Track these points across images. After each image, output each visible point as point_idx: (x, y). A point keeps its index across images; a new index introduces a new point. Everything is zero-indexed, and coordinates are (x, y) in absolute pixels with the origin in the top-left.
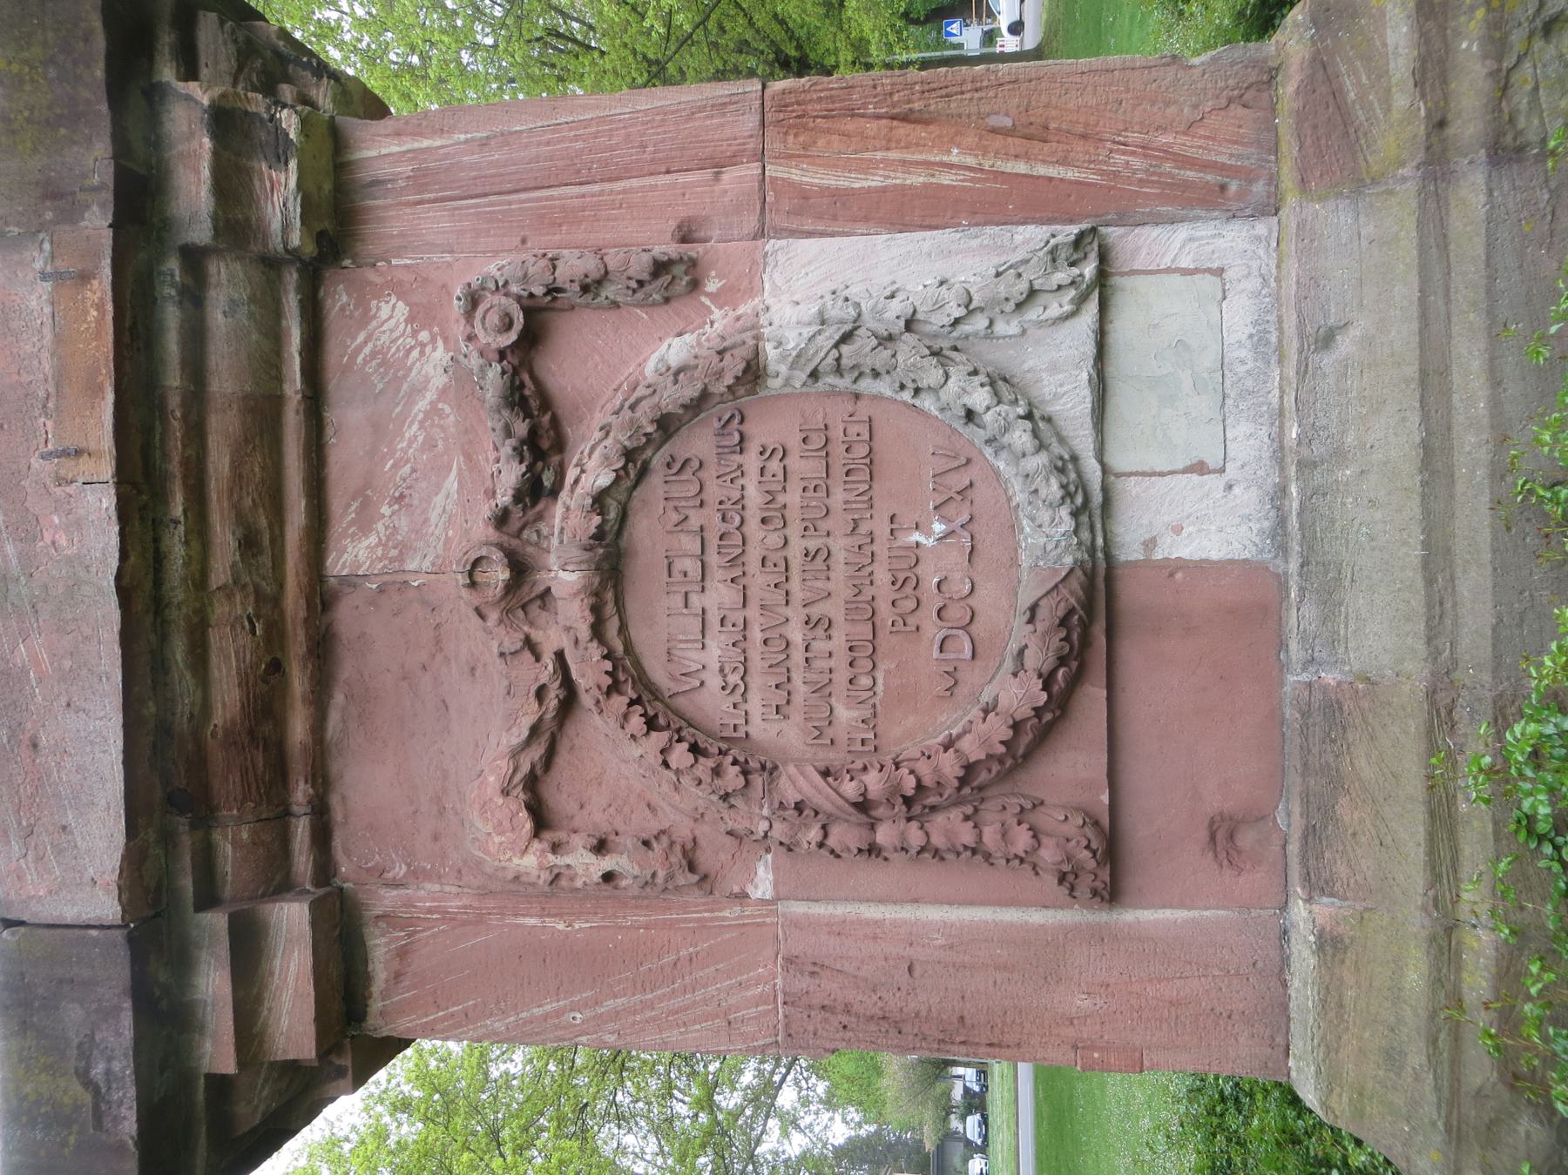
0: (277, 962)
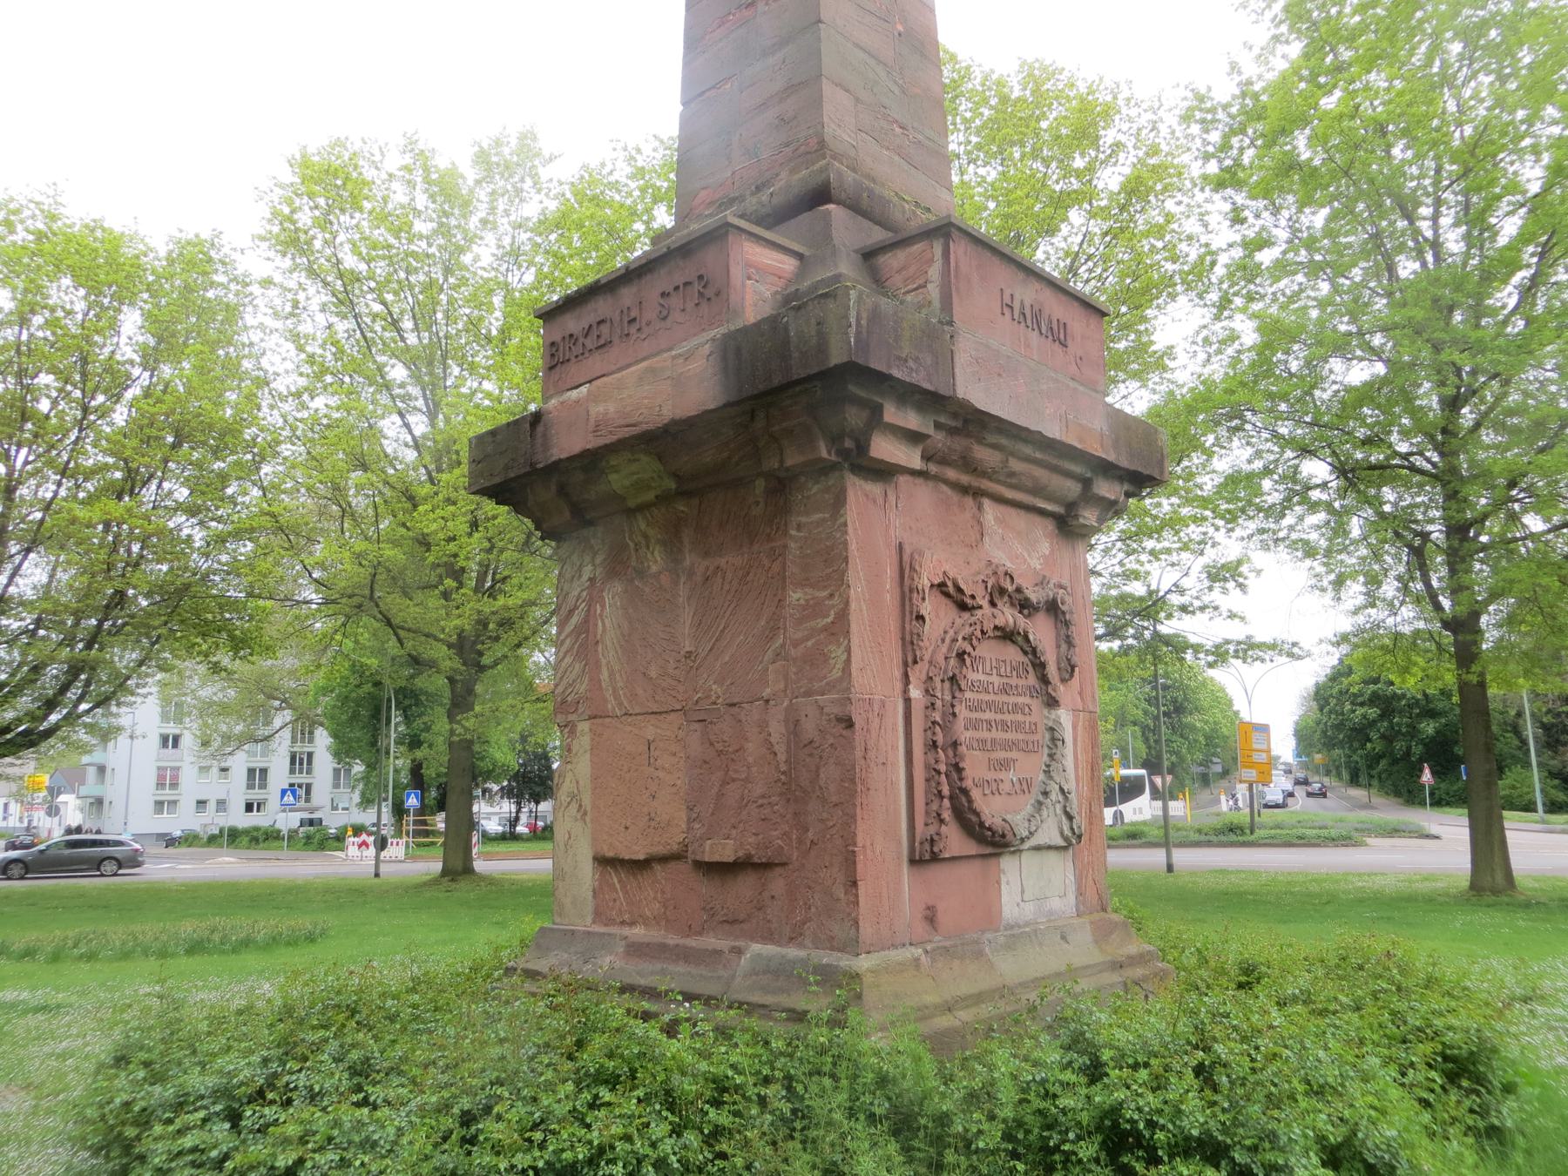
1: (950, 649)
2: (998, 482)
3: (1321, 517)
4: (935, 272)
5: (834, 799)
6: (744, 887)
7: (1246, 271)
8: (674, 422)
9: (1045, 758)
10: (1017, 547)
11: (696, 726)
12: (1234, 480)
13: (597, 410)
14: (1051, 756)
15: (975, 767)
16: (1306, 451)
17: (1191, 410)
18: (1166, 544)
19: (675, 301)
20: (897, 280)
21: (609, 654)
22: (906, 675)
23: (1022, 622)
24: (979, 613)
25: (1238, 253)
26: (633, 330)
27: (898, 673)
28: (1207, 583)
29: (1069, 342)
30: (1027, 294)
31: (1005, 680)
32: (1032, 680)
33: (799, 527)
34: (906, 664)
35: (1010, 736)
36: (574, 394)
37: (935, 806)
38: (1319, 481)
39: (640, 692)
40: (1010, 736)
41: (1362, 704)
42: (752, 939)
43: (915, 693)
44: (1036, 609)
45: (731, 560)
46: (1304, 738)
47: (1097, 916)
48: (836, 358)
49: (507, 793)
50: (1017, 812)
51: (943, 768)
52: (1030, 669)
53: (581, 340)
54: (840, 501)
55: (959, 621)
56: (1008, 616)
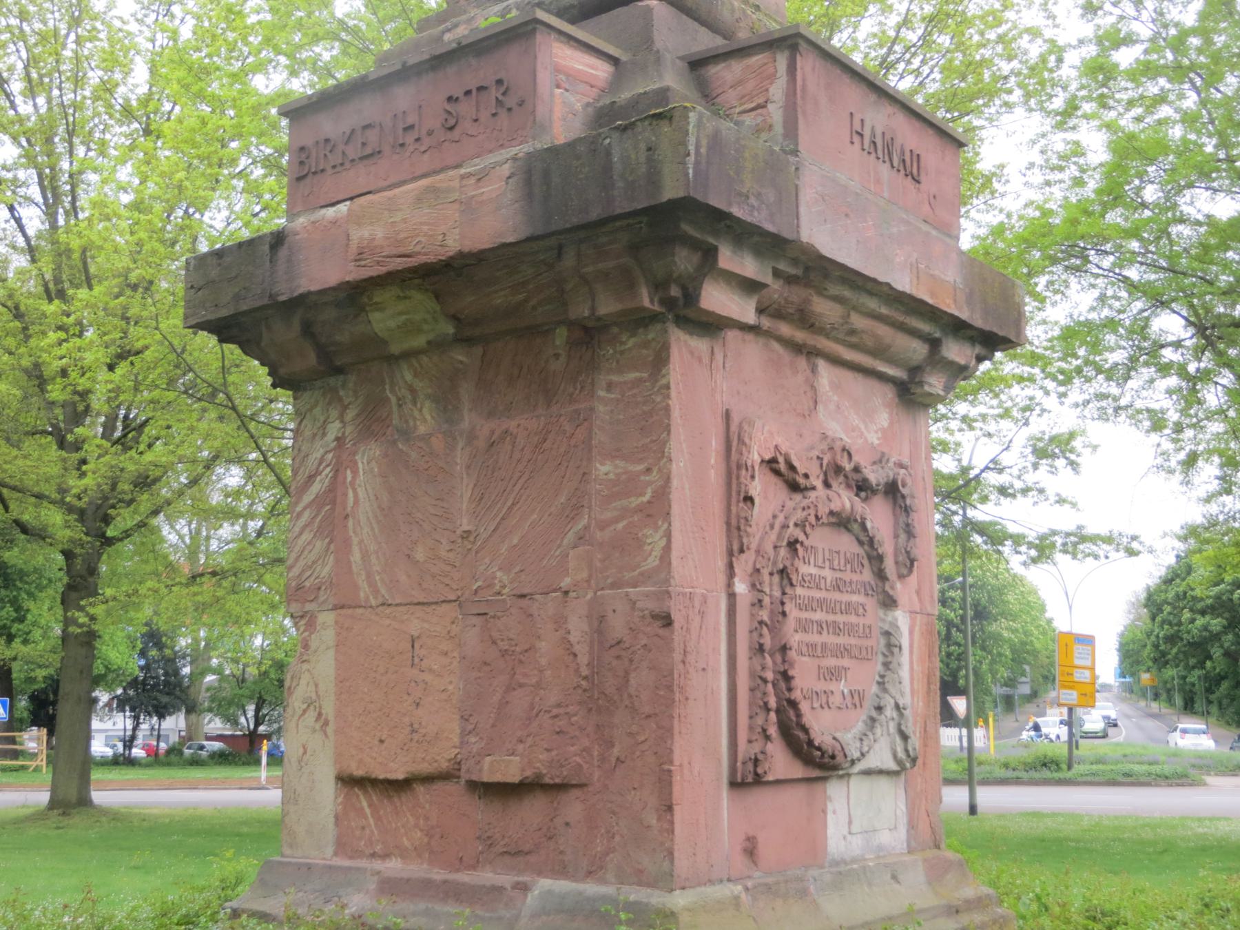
0: (736, 298)
1: (780, 537)
2: (837, 340)
3: (1173, 381)
4: (777, 90)
5: (647, 709)
6: (532, 811)
7: (1100, 72)
8: (461, 255)
9: (880, 668)
10: (853, 417)
11: (475, 620)
12: (1073, 334)
13: (360, 234)
14: (886, 665)
15: (805, 677)
16: (1160, 303)
17: (1028, 243)
18: (982, 409)
19: (465, 109)
20: (730, 97)
21: (363, 528)
22: (730, 566)
23: (860, 507)
24: (812, 494)
25: (1091, 50)
26: (409, 139)
27: (721, 564)
28: (1031, 458)
29: (923, 178)
30: (879, 118)
31: (839, 575)
32: (867, 575)
33: (610, 387)
34: (730, 554)
35: (842, 640)
36: (330, 212)
37: (760, 721)
38: (1171, 338)
39: (403, 578)
40: (842, 640)
41: (1203, 613)
42: (540, 873)
43: (741, 587)
44: (874, 492)
45: (523, 424)
46: (1130, 657)
47: (932, 853)
48: (671, 191)
49: (122, 703)
50: (846, 729)
51: (770, 675)
52: (866, 562)
53: (341, 147)
54: (660, 360)
55: (790, 504)
56: (844, 499)
